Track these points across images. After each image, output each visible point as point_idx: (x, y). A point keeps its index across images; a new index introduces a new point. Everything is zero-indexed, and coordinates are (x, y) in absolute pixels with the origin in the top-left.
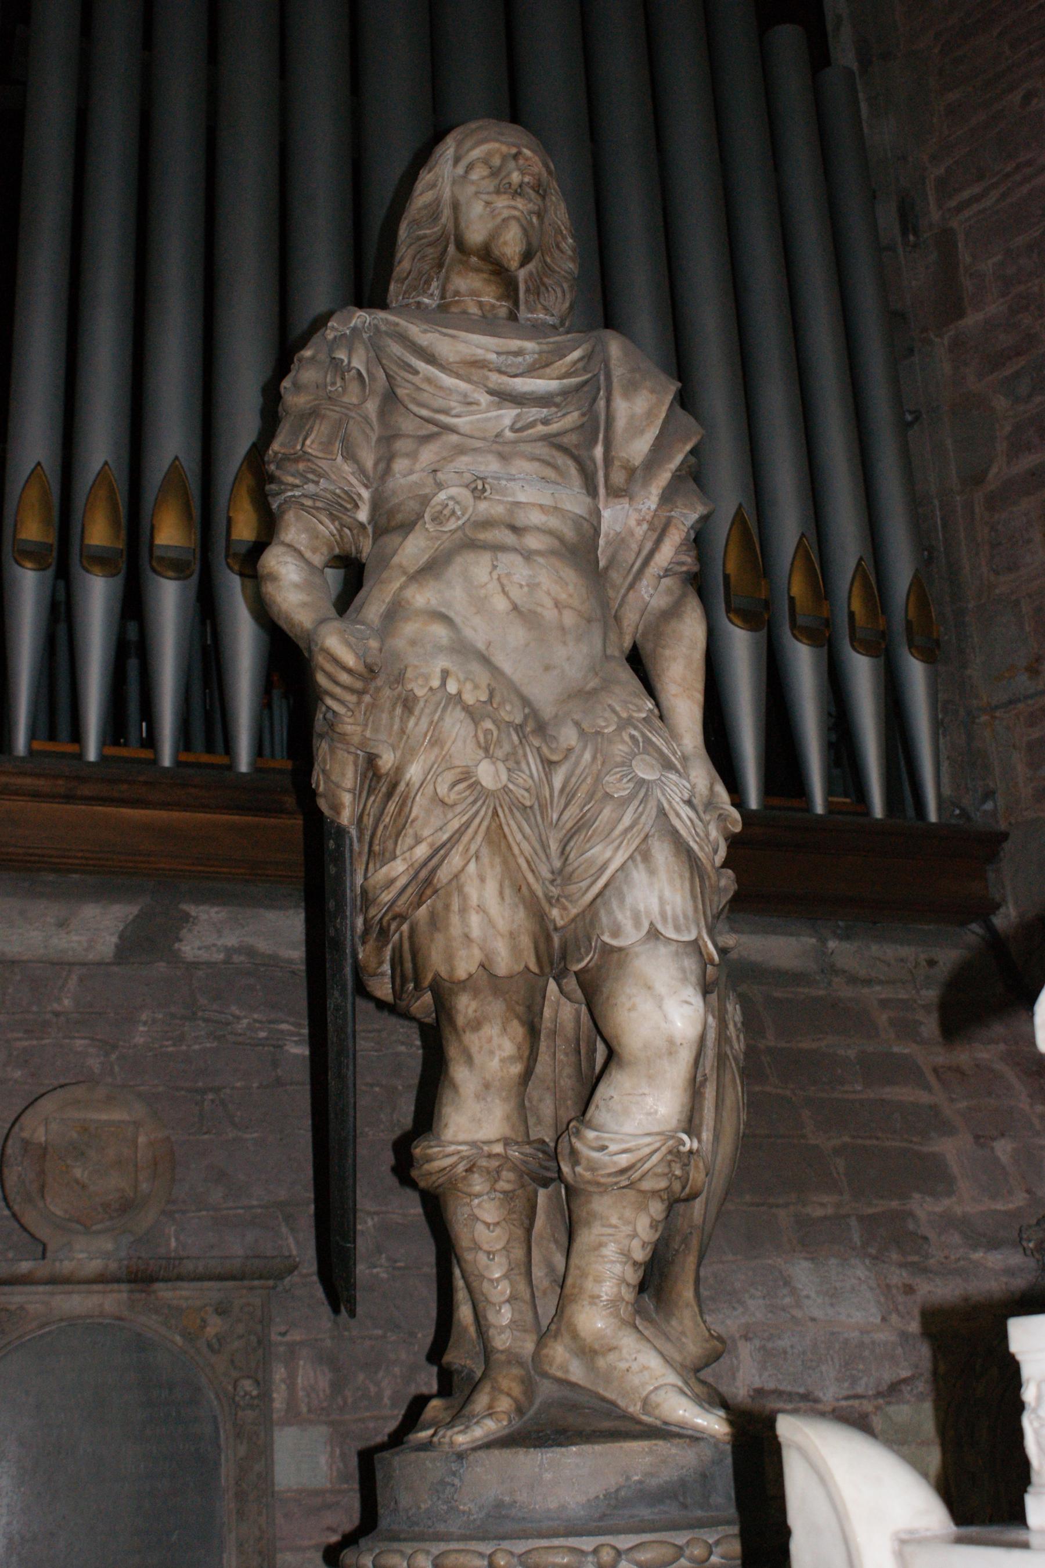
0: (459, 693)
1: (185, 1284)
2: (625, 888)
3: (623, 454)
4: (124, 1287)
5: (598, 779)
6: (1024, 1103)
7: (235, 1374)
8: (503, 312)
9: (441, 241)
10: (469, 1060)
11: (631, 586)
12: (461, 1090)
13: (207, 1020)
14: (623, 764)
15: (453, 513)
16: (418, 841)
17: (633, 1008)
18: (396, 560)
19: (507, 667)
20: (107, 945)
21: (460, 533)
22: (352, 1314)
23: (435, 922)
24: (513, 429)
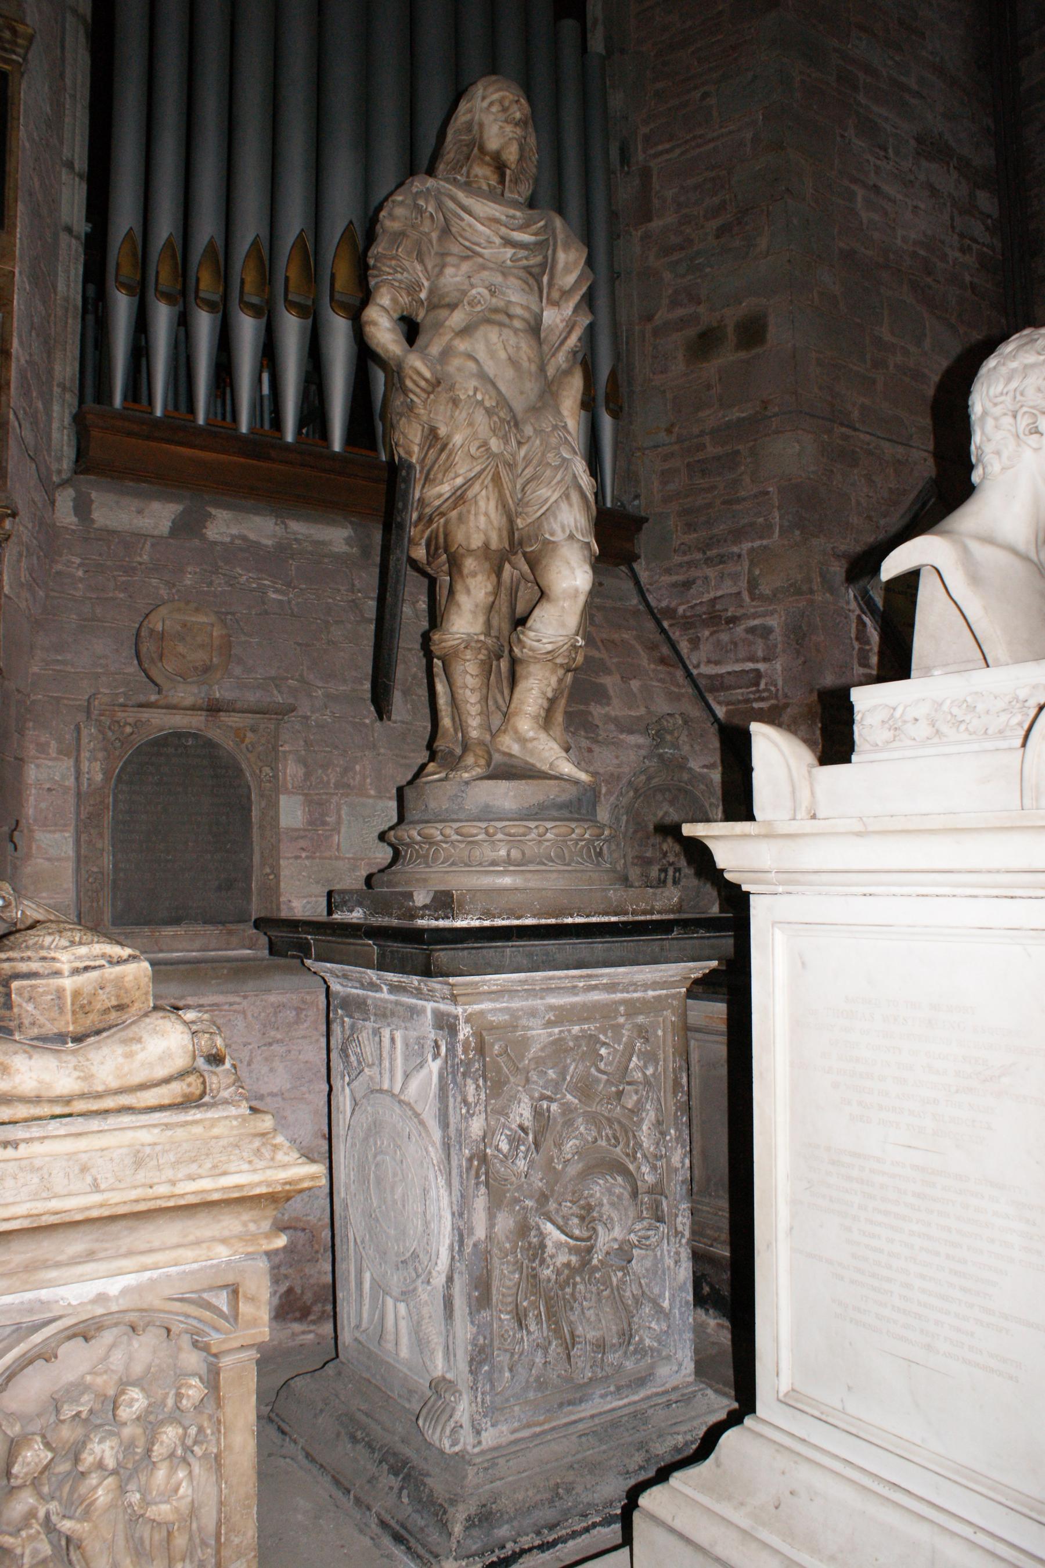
0: (483, 401)
1: (236, 715)
2: (557, 512)
3: (560, 283)
4: (204, 713)
5: (543, 455)
6: (645, 662)
7: (260, 764)
8: (499, 191)
9: (471, 145)
10: (468, 591)
11: (553, 355)
12: (463, 607)
13: (224, 575)
14: (555, 448)
15: (479, 302)
16: (457, 476)
17: (559, 572)
18: (447, 323)
19: (503, 389)
20: (165, 527)
21: (481, 314)
22: (389, 719)
23: (460, 518)
24: (511, 260)
